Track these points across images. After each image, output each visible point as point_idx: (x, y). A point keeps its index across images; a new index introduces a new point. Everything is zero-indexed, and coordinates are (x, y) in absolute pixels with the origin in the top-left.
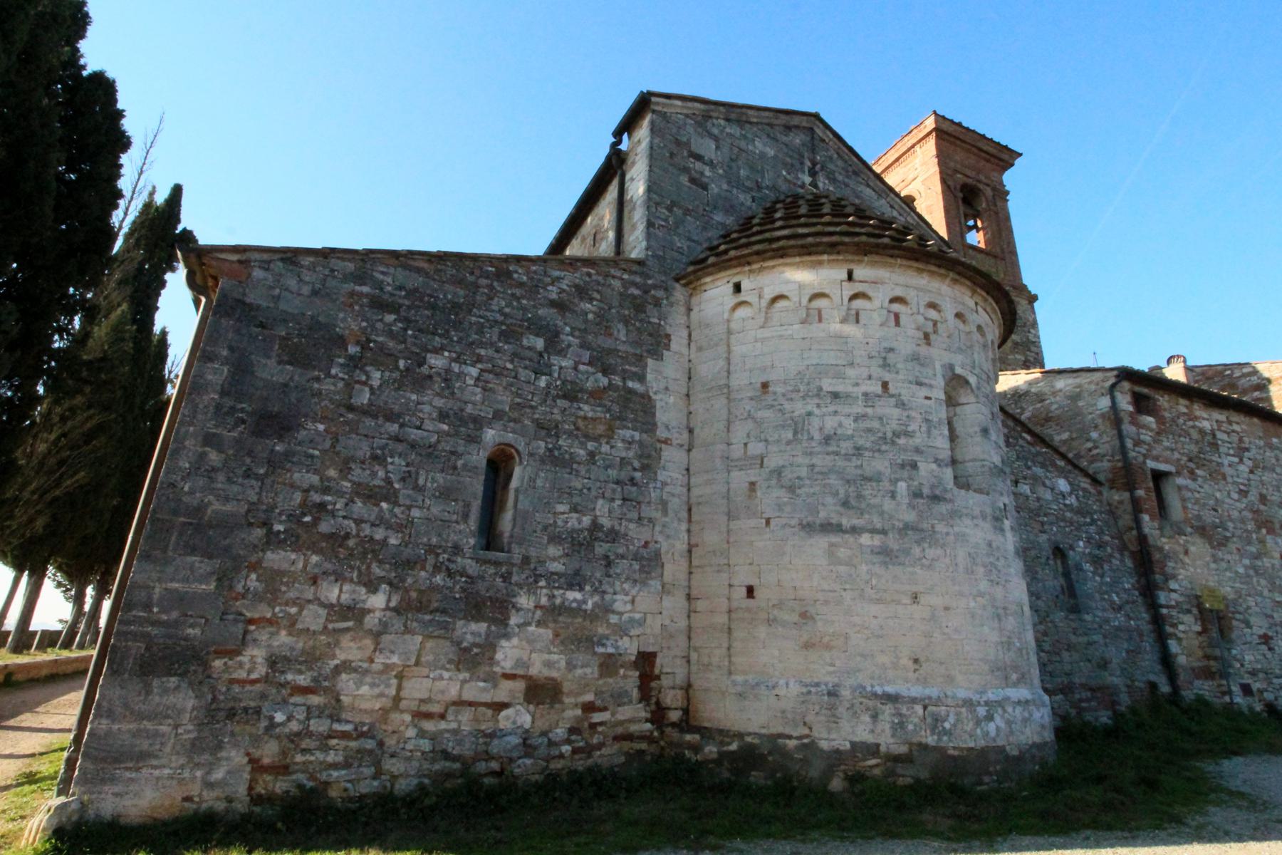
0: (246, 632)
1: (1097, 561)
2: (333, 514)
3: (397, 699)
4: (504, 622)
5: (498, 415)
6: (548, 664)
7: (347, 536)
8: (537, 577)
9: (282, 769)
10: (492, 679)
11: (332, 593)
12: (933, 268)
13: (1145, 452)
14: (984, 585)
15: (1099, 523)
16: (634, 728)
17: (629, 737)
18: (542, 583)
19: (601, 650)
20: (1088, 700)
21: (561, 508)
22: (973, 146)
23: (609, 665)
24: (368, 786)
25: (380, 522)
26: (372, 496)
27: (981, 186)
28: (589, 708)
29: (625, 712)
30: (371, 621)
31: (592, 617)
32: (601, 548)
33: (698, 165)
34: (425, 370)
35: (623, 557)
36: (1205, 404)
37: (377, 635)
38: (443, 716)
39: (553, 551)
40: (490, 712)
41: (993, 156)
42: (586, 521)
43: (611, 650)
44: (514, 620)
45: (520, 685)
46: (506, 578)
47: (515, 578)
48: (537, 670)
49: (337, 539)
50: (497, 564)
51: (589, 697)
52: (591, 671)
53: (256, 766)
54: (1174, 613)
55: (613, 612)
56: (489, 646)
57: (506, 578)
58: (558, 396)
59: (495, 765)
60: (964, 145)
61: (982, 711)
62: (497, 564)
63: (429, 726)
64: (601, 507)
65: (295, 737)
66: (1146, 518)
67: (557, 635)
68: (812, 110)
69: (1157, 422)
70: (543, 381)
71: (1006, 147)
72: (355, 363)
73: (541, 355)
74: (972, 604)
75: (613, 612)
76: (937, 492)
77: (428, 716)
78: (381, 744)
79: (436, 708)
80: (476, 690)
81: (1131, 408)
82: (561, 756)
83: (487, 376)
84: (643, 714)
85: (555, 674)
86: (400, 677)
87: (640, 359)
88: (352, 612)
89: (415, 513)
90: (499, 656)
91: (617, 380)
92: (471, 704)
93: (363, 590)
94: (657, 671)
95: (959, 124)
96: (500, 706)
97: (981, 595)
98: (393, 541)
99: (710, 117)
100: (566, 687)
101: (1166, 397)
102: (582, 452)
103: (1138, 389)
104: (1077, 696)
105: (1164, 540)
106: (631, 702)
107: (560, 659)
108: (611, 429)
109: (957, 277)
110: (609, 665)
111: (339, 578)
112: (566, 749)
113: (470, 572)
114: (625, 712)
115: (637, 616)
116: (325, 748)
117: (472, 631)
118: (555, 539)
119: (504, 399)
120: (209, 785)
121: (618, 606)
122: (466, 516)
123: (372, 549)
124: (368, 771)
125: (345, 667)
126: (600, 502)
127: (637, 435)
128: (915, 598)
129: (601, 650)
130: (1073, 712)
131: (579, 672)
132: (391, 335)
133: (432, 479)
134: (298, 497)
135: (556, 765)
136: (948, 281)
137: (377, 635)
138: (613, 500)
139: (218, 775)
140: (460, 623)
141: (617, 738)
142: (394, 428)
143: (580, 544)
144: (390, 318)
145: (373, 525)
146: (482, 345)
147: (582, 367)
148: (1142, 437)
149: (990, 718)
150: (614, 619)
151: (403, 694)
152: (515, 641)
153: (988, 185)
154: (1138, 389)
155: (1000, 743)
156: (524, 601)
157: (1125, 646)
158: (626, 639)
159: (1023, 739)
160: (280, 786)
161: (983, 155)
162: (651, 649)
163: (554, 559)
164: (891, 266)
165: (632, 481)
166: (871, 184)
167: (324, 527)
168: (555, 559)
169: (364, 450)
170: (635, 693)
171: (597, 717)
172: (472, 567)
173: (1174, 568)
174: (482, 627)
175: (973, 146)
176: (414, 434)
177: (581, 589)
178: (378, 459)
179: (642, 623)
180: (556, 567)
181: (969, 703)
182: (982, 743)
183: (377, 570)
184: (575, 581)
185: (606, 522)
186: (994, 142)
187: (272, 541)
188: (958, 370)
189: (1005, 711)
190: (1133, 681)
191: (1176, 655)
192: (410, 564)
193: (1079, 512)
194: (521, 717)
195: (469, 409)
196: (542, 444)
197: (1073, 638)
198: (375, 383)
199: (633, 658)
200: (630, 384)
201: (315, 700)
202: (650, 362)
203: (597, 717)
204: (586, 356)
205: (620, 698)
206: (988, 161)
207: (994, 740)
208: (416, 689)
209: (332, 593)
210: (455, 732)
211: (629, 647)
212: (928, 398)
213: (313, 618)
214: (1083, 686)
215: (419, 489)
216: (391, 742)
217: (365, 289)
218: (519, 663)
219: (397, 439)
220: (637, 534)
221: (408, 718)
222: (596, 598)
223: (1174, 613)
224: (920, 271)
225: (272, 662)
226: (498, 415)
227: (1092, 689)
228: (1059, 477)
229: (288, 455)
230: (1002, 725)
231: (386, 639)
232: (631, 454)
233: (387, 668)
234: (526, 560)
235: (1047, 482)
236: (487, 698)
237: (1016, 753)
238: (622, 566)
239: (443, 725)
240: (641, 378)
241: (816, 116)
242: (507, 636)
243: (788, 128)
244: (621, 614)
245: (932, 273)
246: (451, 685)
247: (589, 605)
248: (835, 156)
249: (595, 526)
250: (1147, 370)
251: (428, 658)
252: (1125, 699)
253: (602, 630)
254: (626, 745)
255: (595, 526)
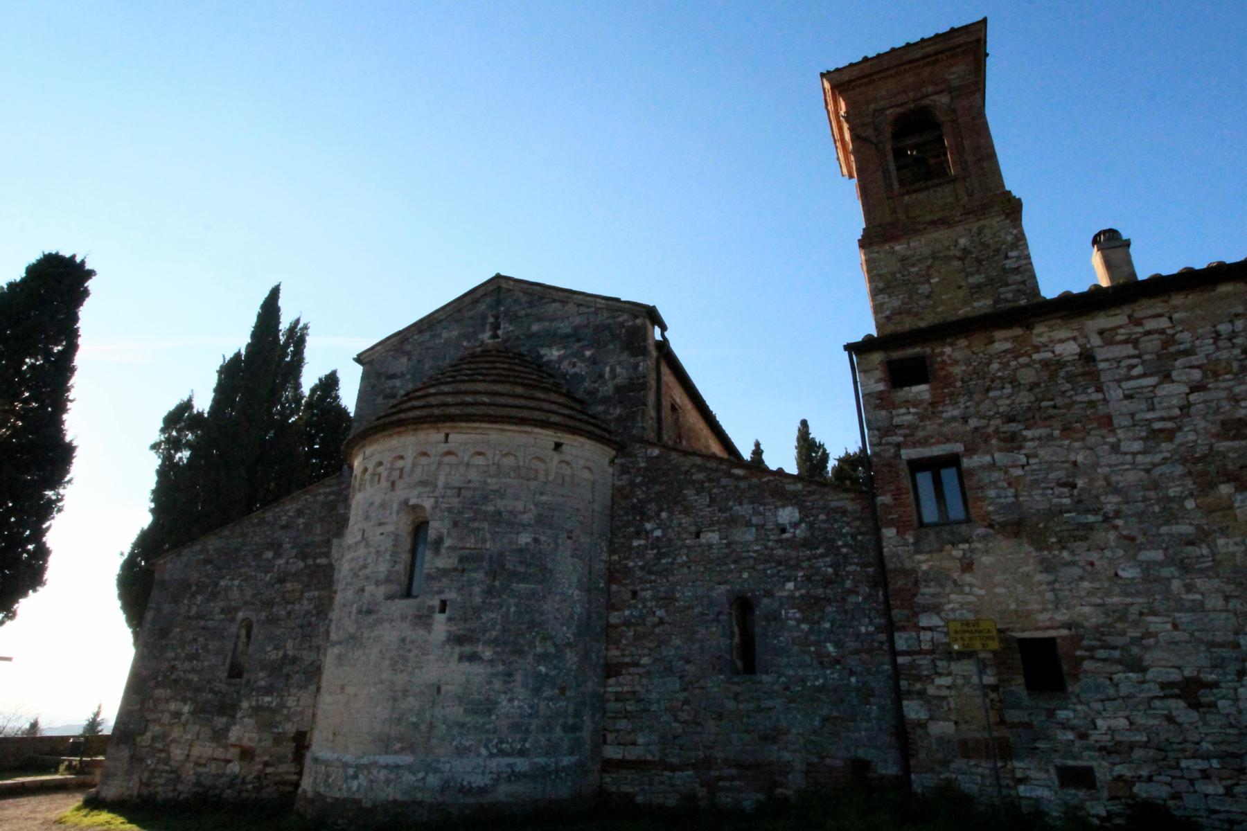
0: (146, 726)
1: (810, 605)
2: (177, 669)
3: (188, 756)
4: (234, 717)
5: (246, 603)
6: (250, 739)
7: (181, 679)
8: (252, 690)
9: (147, 785)
10: (226, 747)
11: (173, 706)
12: (397, 430)
13: (901, 439)
14: (386, 675)
15: (844, 550)
16: (288, 777)
17: (284, 783)
18: (254, 693)
19: (275, 730)
20: (732, 778)
21: (269, 649)
22: (902, 65)
23: (278, 739)
24: (171, 795)
25: (193, 671)
26: (190, 658)
27: (926, 102)
28: (266, 764)
29: (282, 768)
30: (183, 718)
31: (274, 711)
32: (286, 669)
33: (391, 383)
34: (218, 589)
35: (297, 672)
36: (1062, 318)
37: (184, 725)
38: (205, 765)
39: (261, 675)
40: (223, 764)
41: (936, 53)
42: (281, 653)
43: (280, 730)
44: (239, 715)
45: (237, 750)
46: (238, 693)
47: (242, 692)
48: (245, 742)
49: (176, 681)
50: (235, 685)
51: (266, 758)
52: (269, 743)
53: (142, 783)
54: (924, 661)
55: (285, 707)
56: (226, 730)
57: (238, 693)
58: (275, 583)
59: (217, 792)
60: (889, 73)
61: (351, 771)
62: (235, 685)
63: (200, 770)
64: (289, 644)
65: (153, 771)
66: (889, 533)
67: (257, 722)
68: (493, 275)
69: (932, 389)
70: (268, 578)
71: (953, 30)
72: (193, 595)
73: (270, 561)
74: (373, 690)
75: (285, 707)
76: (371, 607)
77: (200, 765)
78: (179, 777)
79: (203, 761)
80: (220, 753)
81: (881, 387)
82: (247, 791)
83: (243, 583)
84: (292, 770)
85: (252, 745)
86: (190, 746)
87: (328, 543)
88: (177, 715)
89: (206, 664)
90: (230, 735)
91: (310, 561)
92: (215, 759)
93: (182, 704)
94: (306, 743)
95: (866, 59)
96: (228, 761)
97: (382, 682)
98: (196, 679)
99: (407, 339)
100: (258, 751)
101: (963, 343)
102: (284, 613)
103: (896, 355)
104: (714, 773)
105: (919, 557)
106: (286, 762)
107: (255, 736)
108: (302, 592)
109: (414, 427)
110: (278, 739)
111: (174, 698)
112: (250, 786)
113: (224, 691)
114: (282, 768)
115: (299, 709)
116: (161, 777)
117: (221, 721)
118: (263, 668)
119: (249, 593)
120: (128, 788)
121: (289, 704)
122: (224, 662)
123: (189, 683)
124: (170, 788)
125: (174, 741)
126: (289, 641)
127: (316, 593)
128: (343, 688)
129: (275, 730)
130: (702, 792)
131: (263, 744)
132: (207, 576)
133: (214, 645)
134: (167, 663)
135: (244, 795)
136: (410, 433)
137: (184, 725)
138: (295, 639)
139: (131, 785)
140: (216, 718)
141: (276, 783)
142: (202, 623)
143: (275, 669)
144: (209, 566)
145: (190, 672)
146: (240, 568)
147: (291, 561)
148: (896, 421)
149: (355, 777)
150: (285, 711)
151: (192, 753)
152: (238, 727)
153: (941, 92)
154: (896, 355)
155: (357, 796)
156: (245, 705)
157: (825, 712)
158: (291, 723)
159: (382, 796)
160: (145, 792)
161: (922, 62)
162: (305, 729)
163: (262, 679)
164: (376, 441)
165: (310, 624)
166: (557, 298)
167: (174, 677)
168: (262, 678)
169: (190, 636)
170: (290, 756)
171: (269, 770)
172: (223, 687)
173: (933, 595)
174: (224, 720)
175: (902, 65)
176: (210, 624)
177: (272, 695)
178: (195, 640)
179: (302, 713)
180: (263, 683)
181: (346, 765)
182: (345, 795)
183: (188, 694)
184: (269, 691)
185: (290, 653)
186: (916, 44)
187: (158, 685)
188: (413, 501)
189: (370, 772)
190: (822, 758)
191: (922, 725)
192: (198, 690)
193: (806, 543)
194: (235, 768)
195: (233, 604)
196: (264, 614)
197: (730, 705)
198: (199, 602)
199: (292, 735)
200: (318, 561)
201: (163, 755)
202: (335, 541)
203: (269, 770)
204: (294, 552)
205: (281, 759)
206: (935, 62)
207: (354, 794)
208: (196, 751)
209: (173, 706)
210: (207, 773)
211: (290, 728)
212: (382, 534)
213: (166, 718)
214: (727, 762)
215: (208, 651)
216: (183, 776)
217: (202, 557)
218: (239, 739)
219: (203, 628)
220: (308, 656)
221: (192, 765)
222: (279, 700)
223: (924, 661)
224: (391, 436)
225: (152, 739)
226: (246, 603)
227: (740, 766)
228: (784, 506)
229: (167, 645)
230: (364, 784)
231: (189, 726)
232: (311, 606)
233: (187, 740)
234: (248, 681)
235: (755, 520)
236: (222, 757)
237: (369, 805)
238: (296, 678)
239: (205, 770)
240: (327, 555)
241: (498, 277)
242: (235, 724)
243: (476, 302)
244: (290, 708)
245: (398, 433)
246: (204, 749)
247: (274, 704)
248: (521, 295)
249: (285, 656)
250: (16, 606)
251: (202, 736)
252: (795, 783)
253: (278, 718)
254: (281, 788)
255: (285, 656)
